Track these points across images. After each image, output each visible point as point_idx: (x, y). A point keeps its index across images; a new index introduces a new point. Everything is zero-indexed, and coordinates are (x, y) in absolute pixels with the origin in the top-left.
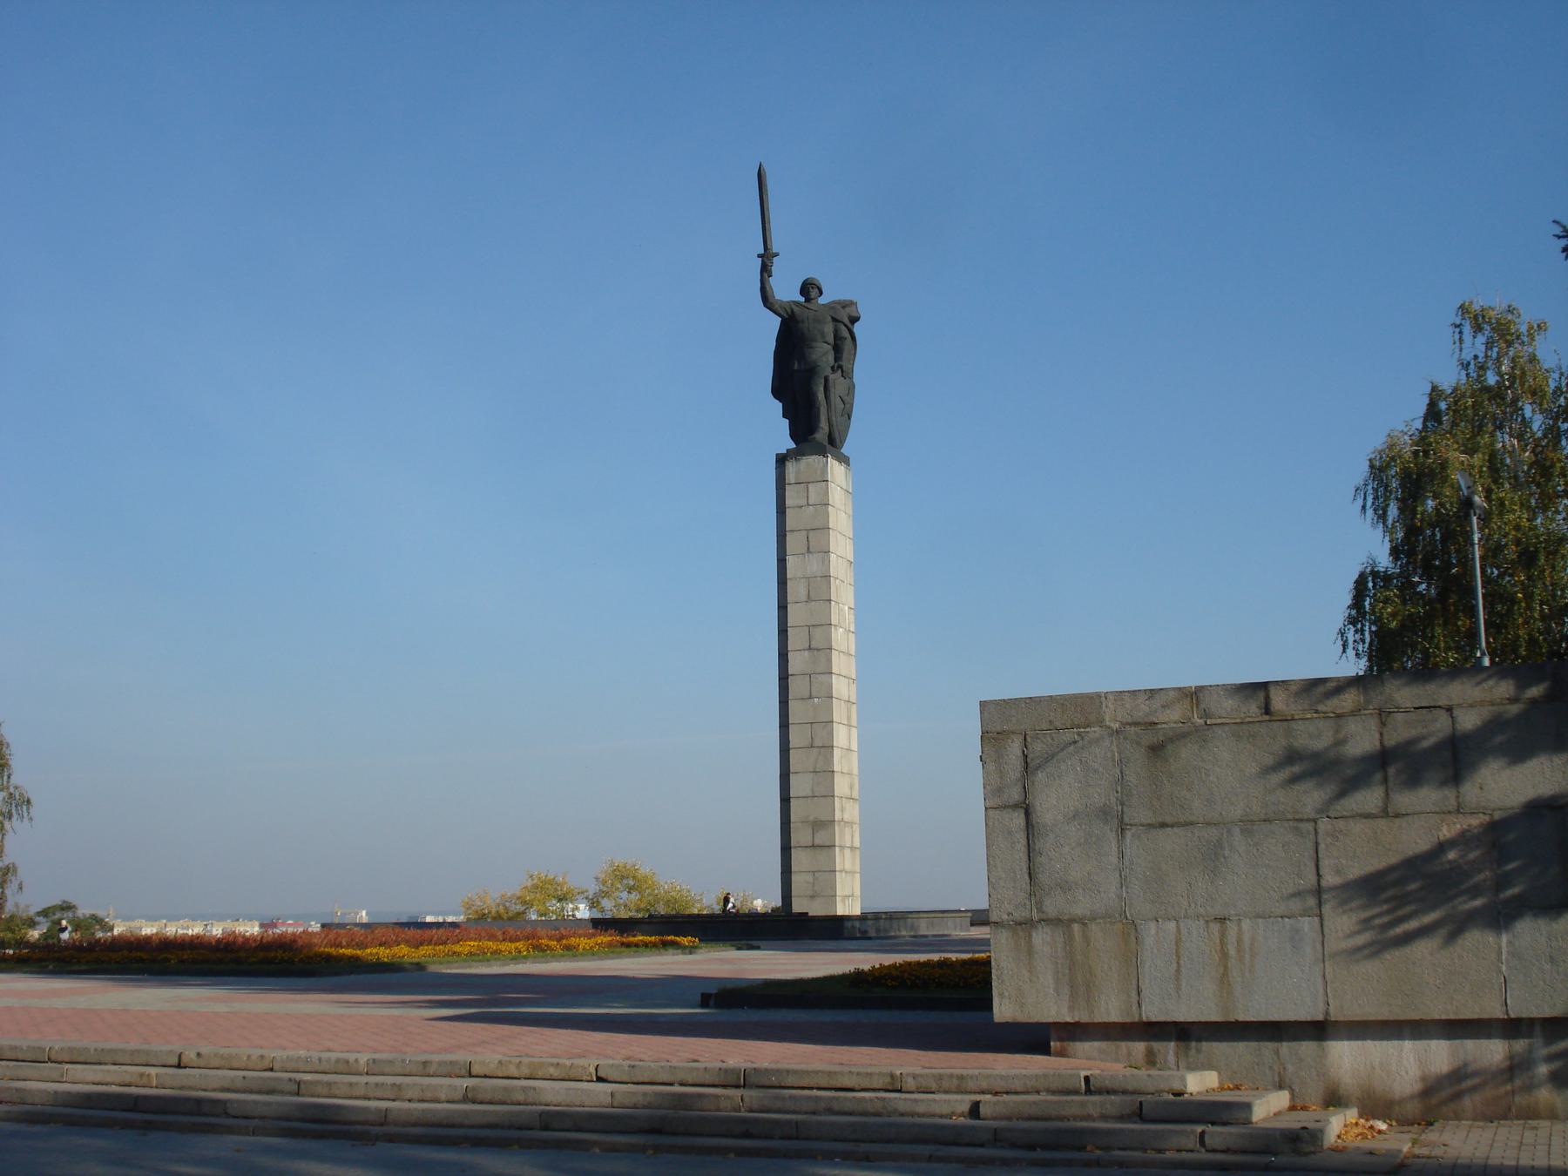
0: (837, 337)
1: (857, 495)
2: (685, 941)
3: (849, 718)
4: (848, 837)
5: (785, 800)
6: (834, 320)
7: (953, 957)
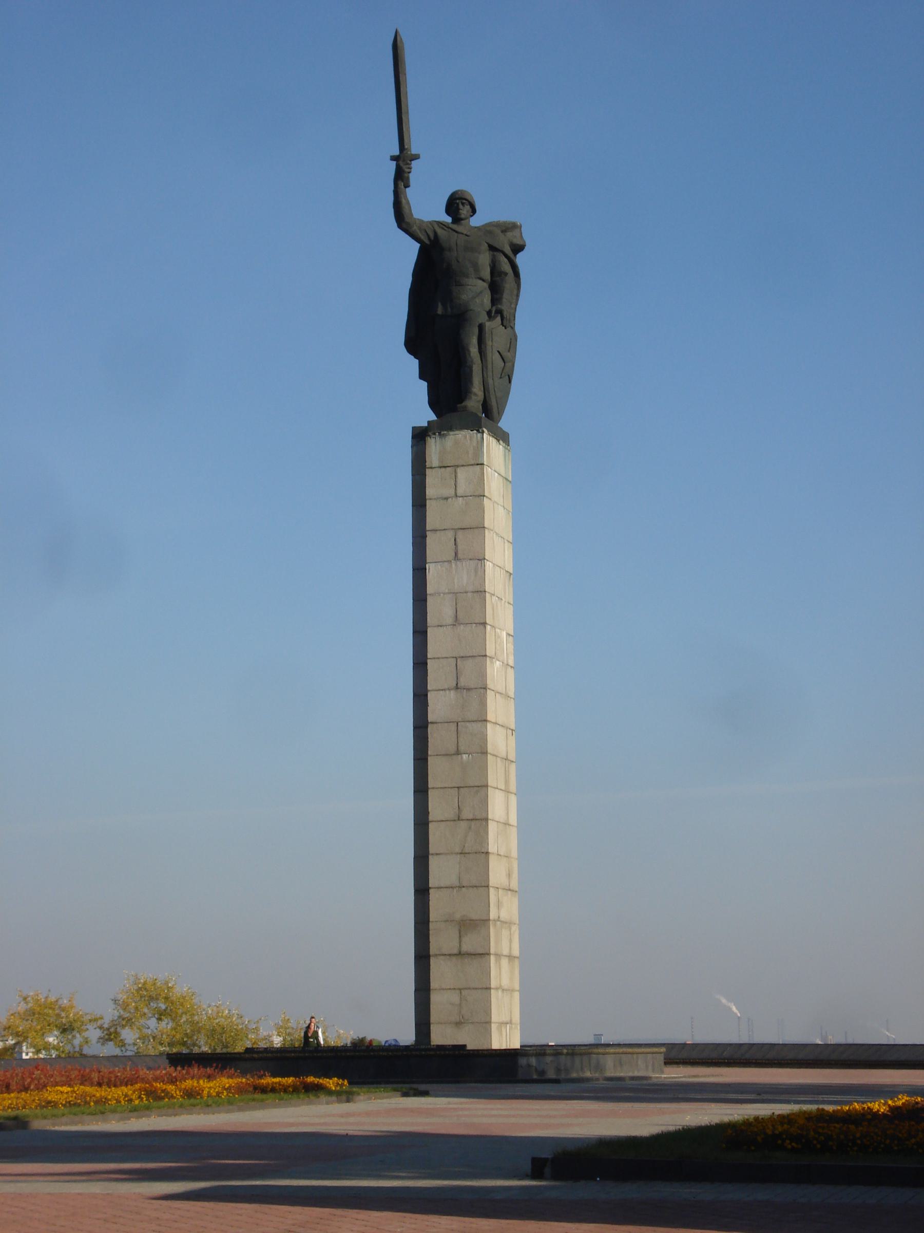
0: (495, 270)
1: (517, 484)
2: (331, 1083)
3: (507, 782)
4: (505, 942)
5: (422, 891)
6: (492, 248)
7: (830, 1108)
